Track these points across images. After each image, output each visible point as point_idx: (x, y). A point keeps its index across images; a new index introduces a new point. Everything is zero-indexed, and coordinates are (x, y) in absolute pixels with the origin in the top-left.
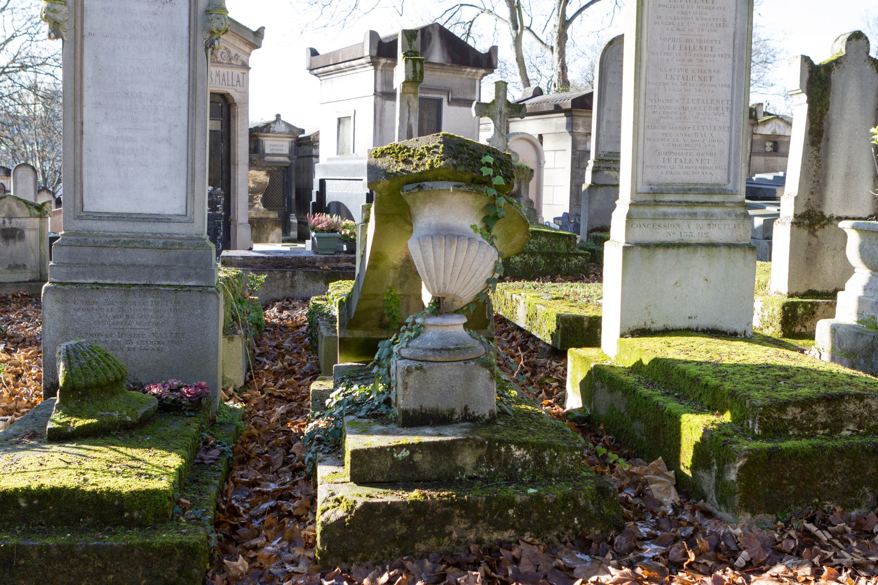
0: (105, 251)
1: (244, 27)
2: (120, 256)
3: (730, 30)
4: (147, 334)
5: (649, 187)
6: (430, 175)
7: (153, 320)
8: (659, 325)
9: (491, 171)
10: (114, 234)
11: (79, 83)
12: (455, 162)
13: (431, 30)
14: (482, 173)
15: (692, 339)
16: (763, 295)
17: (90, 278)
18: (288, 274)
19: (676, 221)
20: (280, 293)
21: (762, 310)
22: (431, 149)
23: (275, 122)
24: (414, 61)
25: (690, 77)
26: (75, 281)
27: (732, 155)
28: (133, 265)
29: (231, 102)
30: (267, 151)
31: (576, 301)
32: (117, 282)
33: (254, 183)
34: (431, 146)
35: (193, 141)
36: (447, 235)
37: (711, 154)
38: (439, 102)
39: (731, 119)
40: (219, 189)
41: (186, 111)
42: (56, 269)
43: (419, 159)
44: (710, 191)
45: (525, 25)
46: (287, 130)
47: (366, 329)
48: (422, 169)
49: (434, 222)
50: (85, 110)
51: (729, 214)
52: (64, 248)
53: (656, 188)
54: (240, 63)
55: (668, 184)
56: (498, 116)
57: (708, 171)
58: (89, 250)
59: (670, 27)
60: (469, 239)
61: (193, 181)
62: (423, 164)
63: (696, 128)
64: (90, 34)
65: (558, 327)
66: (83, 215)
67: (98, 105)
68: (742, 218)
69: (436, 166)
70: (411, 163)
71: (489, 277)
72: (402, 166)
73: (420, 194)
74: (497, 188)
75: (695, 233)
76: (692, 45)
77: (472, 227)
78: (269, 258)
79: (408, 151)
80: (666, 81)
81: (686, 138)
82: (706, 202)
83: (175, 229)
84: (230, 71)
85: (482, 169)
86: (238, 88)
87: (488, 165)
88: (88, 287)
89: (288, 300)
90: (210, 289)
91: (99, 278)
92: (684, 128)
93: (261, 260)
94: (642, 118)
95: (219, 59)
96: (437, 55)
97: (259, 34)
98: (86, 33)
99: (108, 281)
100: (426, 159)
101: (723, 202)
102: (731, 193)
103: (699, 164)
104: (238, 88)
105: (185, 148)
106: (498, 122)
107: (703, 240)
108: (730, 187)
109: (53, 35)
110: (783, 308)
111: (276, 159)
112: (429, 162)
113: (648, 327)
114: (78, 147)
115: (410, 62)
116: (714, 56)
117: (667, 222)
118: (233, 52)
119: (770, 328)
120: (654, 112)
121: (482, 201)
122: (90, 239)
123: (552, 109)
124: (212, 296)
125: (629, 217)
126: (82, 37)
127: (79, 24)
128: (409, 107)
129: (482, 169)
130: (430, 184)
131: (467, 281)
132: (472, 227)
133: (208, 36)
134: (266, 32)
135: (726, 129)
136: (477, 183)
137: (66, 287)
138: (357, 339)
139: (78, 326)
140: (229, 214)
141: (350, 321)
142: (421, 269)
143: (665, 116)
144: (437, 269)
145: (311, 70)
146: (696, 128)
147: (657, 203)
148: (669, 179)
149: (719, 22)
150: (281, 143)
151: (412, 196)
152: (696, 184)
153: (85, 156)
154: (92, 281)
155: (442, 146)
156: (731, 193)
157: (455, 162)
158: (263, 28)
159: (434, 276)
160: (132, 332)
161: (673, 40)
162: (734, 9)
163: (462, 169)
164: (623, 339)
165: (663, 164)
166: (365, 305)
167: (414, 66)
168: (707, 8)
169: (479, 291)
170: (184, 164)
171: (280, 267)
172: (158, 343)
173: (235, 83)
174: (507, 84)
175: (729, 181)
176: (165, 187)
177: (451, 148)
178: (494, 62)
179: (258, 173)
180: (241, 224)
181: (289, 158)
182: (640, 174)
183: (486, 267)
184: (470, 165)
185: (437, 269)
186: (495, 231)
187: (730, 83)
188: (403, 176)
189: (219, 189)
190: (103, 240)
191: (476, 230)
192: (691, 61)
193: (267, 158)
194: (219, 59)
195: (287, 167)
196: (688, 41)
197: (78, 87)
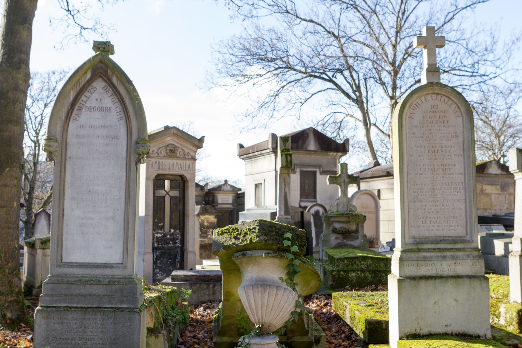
0: (73, 287)
1: (193, 137)
2: (82, 290)
3: (460, 140)
4: (96, 339)
5: (414, 240)
6: (251, 246)
7: (100, 330)
8: (425, 331)
9: (289, 243)
10: (79, 276)
11: (62, 186)
12: (266, 238)
13: (308, 132)
14: (284, 244)
15: (446, 342)
16: (506, 303)
17: (64, 303)
18: (211, 286)
19: (433, 262)
20: (206, 298)
21: (505, 314)
22: (251, 230)
23: (224, 185)
24: (286, 155)
25: (436, 169)
26: (55, 305)
27: (468, 218)
28: (90, 295)
29: (185, 179)
30: (220, 202)
31: (381, 308)
32: (79, 306)
33: (208, 222)
34: (251, 228)
35: (128, 218)
36: (263, 284)
37: (454, 217)
38: (315, 173)
39: (465, 195)
40: (178, 231)
41: (124, 201)
42: (44, 298)
43: (244, 236)
44: (454, 241)
45: (372, 122)
46: (231, 189)
47: (230, 336)
48: (245, 243)
49: (254, 276)
50: (66, 201)
51: (468, 256)
52: (49, 285)
53: (418, 240)
54: (190, 157)
55: (426, 238)
56: (343, 184)
57: (452, 228)
58: (63, 286)
59: (421, 139)
60: (277, 287)
61: (127, 243)
62: (246, 240)
63: (442, 201)
64: (70, 158)
65: (366, 328)
66: (62, 264)
67: (73, 199)
68: (477, 258)
69: (254, 241)
70: (238, 239)
71: (292, 310)
72: (233, 241)
73: (244, 259)
74: (294, 253)
75: (446, 269)
76: (436, 149)
77: (280, 278)
78: (200, 276)
79: (238, 231)
80: (421, 172)
81: (437, 208)
82: (452, 249)
83: (116, 272)
84: (184, 162)
85: (285, 242)
86: (189, 172)
87: (288, 239)
88: (62, 309)
89: (210, 302)
90: (135, 310)
91: (69, 303)
92: (435, 202)
93: (195, 277)
94: (406, 196)
95: (178, 155)
96: (312, 145)
97: (201, 140)
98: (68, 158)
99: (75, 305)
100: (248, 236)
101: (464, 248)
102: (469, 242)
103: (446, 224)
104: (189, 172)
105: (123, 223)
106: (343, 187)
107: (452, 273)
108: (468, 238)
109: (48, 159)
110: (518, 313)
111: (225, 206)
112: (250, 238)
113: (418, 332)
114: (61, 224)
115: (284, 156)
116: (451, 156)
117: (427, 262)
118: (187, 151)
119: (511, 326)
120: (414, 192)
121: (284, 262)
122: (65, 280)
123: (385, 174)
124: (136, 315)
125: (401, 260)
126: (66, 159)
127: (64, 152)
128: (285, 182)
129: (285, 242)
130: (249, 252)
131: (276, 314)
132: (280, 278)
133: (137, 156)
134: (205, 139)
135: (463, 201)
136: (281, 251)
137: (49, 309)
138: (225, 343)
139: (55, 334)
140: (184, 246)
141: (219, 331)
142: (246, 307)
143: (422, 194)
144: (256, 307)
145: (240, 156)
146: (442, 201)
147: (419, 250)
148: (427, 234)
149: (453, 135)
150: (228, 197)
151: (239, 260)
152: (445, 237)
153: (64, 229)
154: (65, 305)
155: (258, 228)
156: (469, 242)
157: (266, 238)
158: (204, 137)
159: (255, 311)
160: (87, 337)
161: (424, 147)
162: (462, 126)
163: (271, 242)
164: (401, 341)
165: (423, 225)
166: (226, 322)
167: (287, 158)
168: (444, 127)
169: (287, 320)
170: (122, 232)
171: (207, 281)
172: (103, 344)
173: (187, 169)
174: (347, 164)
175: (467, 234)
176: (111, 247)
177: (264, 229)
178: (347, 149)
179: (210, 217)
180: (190, 252)
181: (233, 205)
182: (407, 232)
183: (289, 305)
184: (276, 239)
185: (256, 307)
186: (296, 280)
187: (463, 172)
188: (234, 247)
189: (178, 231)
190: (73, 279)
191: (282, 281)
192: (436, 159)
193: (220, 206)
194: (178, 155)
195: (231, 211)
196: (433, 147)
197: (62, 188)
